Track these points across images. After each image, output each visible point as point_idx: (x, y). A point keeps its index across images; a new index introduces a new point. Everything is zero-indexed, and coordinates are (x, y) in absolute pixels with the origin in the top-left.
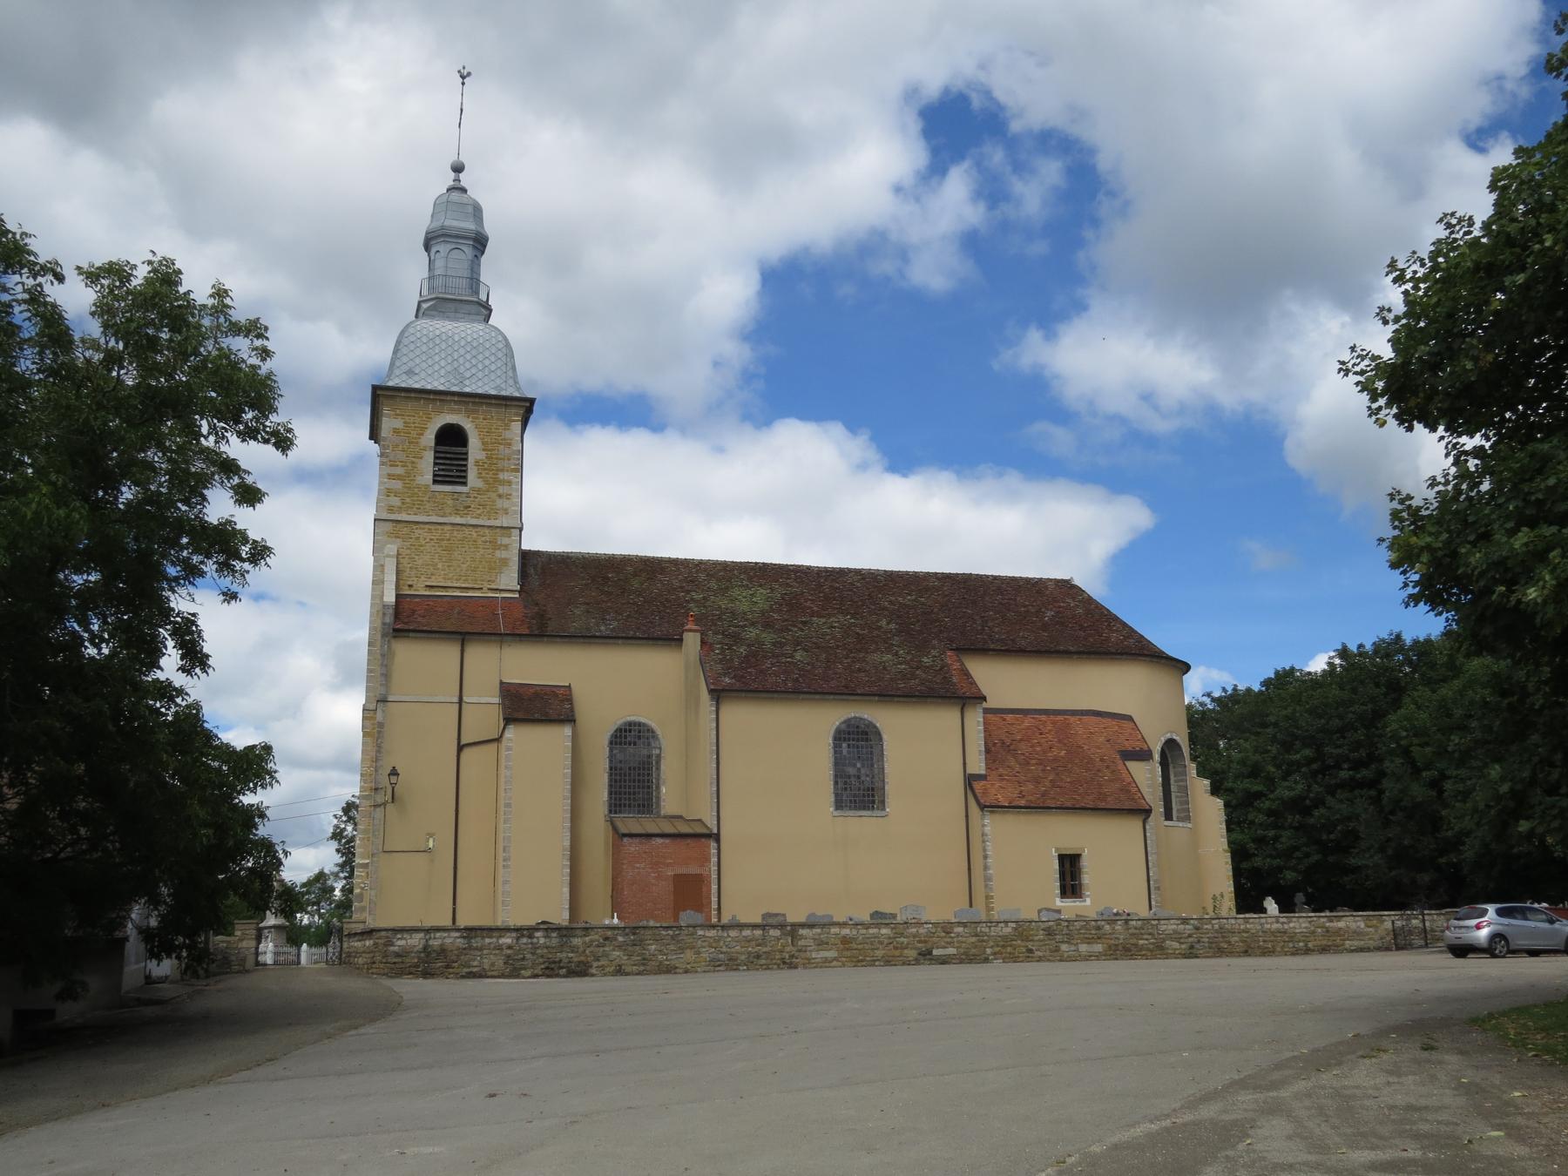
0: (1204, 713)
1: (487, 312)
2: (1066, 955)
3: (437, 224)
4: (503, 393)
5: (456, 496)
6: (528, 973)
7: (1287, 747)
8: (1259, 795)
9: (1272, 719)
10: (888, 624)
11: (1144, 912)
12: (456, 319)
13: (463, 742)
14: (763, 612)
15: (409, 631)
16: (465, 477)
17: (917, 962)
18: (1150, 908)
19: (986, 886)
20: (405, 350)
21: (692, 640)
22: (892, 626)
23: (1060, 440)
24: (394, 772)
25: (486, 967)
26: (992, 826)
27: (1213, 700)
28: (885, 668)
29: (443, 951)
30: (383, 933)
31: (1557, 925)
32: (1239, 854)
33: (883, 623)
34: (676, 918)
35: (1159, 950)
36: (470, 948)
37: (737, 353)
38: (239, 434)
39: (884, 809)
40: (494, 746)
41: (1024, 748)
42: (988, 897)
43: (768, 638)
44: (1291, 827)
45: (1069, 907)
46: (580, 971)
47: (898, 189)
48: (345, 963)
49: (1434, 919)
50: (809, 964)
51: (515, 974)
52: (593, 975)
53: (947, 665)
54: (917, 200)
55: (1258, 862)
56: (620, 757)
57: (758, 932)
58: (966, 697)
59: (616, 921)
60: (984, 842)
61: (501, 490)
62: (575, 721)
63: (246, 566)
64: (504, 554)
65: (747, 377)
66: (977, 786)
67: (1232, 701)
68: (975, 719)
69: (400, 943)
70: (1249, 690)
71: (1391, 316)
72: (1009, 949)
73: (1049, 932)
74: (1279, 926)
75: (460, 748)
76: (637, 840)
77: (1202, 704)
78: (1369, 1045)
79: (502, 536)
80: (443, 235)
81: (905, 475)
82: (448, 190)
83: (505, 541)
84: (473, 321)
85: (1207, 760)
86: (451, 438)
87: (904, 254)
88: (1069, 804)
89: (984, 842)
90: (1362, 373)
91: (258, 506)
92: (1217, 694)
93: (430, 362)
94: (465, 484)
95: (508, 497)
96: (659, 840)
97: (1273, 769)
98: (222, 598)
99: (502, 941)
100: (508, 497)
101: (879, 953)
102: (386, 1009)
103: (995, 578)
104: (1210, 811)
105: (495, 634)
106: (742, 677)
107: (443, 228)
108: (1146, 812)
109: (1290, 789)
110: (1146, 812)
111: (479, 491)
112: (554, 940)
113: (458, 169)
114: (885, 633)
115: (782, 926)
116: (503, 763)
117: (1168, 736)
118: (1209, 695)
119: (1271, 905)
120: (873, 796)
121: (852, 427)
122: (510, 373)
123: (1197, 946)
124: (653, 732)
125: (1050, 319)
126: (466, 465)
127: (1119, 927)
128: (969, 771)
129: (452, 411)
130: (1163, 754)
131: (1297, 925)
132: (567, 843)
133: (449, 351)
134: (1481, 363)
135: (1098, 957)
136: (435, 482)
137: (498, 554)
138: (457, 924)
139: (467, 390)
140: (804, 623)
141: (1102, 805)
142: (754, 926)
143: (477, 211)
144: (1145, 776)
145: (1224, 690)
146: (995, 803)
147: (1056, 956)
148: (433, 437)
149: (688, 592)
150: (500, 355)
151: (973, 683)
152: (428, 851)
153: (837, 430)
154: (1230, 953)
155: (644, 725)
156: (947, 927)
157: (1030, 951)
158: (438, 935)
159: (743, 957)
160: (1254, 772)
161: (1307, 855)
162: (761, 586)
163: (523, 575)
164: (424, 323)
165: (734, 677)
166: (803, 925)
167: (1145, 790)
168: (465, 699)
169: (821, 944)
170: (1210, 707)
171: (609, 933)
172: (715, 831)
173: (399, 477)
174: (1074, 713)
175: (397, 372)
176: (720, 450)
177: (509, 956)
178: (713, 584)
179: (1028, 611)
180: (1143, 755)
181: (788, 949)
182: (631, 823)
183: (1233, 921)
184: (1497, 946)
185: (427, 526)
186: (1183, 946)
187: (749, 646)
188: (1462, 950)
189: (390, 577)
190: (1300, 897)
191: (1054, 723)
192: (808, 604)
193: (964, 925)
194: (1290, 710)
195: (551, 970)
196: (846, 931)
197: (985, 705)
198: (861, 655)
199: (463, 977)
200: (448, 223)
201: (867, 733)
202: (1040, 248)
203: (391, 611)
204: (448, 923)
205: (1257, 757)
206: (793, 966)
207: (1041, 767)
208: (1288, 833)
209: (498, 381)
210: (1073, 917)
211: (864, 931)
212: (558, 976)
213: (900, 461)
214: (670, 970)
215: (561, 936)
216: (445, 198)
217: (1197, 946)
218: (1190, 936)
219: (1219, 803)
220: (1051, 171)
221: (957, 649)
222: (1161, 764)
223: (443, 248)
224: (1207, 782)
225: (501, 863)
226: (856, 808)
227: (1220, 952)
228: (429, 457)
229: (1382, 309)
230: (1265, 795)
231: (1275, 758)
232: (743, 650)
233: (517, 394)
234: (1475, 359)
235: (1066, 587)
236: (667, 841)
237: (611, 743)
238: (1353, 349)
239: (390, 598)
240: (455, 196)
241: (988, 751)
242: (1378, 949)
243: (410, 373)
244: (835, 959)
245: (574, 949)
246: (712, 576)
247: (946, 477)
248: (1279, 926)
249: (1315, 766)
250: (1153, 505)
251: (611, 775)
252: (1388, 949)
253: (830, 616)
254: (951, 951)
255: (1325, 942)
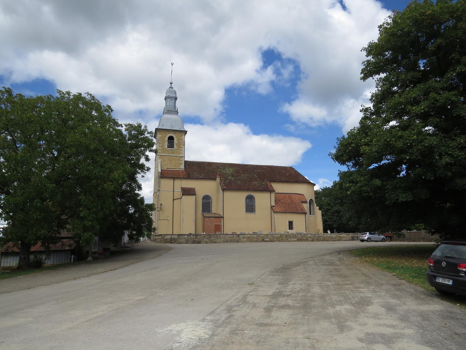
0: (319, 192)
1: (177, 113)
2: (289, 241)
3: (167, 95)
4: (181, 130)
5: (172, 150)
6: (190, 243)
7: (335, 200)
8: (330, 209)
9: (333, 194)
10: (256, 176)
11: (305, 233)
12: (171, 114)
13: (174, 199)
14: (232, 173)
15: (164, 177)
16: (174, 146)
17: (261, 241)
18: (306, 232)
19: (275, 227)
20: (162, 121)
21: (218, 179)
22: (257, 176)
23: (292, 128)
24: (161, 205)
25: (182, 242)
26: (276, 215)
27: (322, 189)
28: (256, 185)
29: (174, 239)
30: (163, 235)
31: (380, 236)
32: (324, 222)
33: (255, 176)
34: (215, 233)
35: (307, 240)
36: (179, 238)
37: (220, 108)
38: (149, 151)
39: (255, 212)
40: (180, 199)
41: (282, 201)
42: (275, 229)
43: (233, 179)
44: (336, 216)
45: (290, 231)
46: (199, 242)
47: (257, 71)
48: (154, 241)
49: (359, 235)
50: (241, 242)
51: (187, 243)
52: (202, 243)
53: (268, 184)
54: (261, 73)
55: (329, 223)
56: (204, 202)
57: (232, 236)
58: (271, 191)
59: (205, 233)
60: (274, 219)
61: (181, 149)
62: (196, 195)
63: (146, 171)
64: (181, 162)
65: (222, 113)
66: (273, 208)
67: (325, 190)
68: (273, 195)
69: (166, 237)
70: (329, 188)
71: (336, 147)
72: (279, 239)
73: (286, 236)
74: (330, 236)
75: (174, 200)
76: (208, 218)
77: (319, 190)
78: (331, 254)
79: (181, 158)
80: (169, 97)
81: (258, 136)
82: (169, 88)
83: (182, 159)
84: (175, 115)
85: (319, 202)
86: (171, 138)
87: (257, 85)
88: (291, 212)
89: (274, 219)
90: (332, 156)
91: (149, 161)
92: (322, 188)
93: (167, 123)
94: (174, 148)
95: (182, 150)
96: (212, 218)
97: (332, 204)
98: (141, 177)
99: (185, 237)
100: (182, 150)
101: (254, 240)
102: (170, 249)
103: (277, 166)
104: (318, 213)
105: (180, 178)
106: (228, 186)
107: (169, 96)
108: (306, 213)
109: (336, 208)
110: (306, 213)
111: (176, 149)
112: (194, 237)
113: (171, 83)
114: (256, 178)
115: (236, 235)
116: (182, 203)
117: (311, 198)
118: (321, 188)
119: (329, 232)
120: (253, 210)
121: (245, 125)
122: (182, 126)
123: (314, 239)
124: (211, 197)
125: (290, 100)
126: (174, 144)
127: (299, 235)
128: (271, 205)
129: (171, 133)
130: (310, 202)
131: (333, 236)
132: (194, 218)
133: (170, 121)
134: (346, 158)
135: (295, 241)
136: (168, 147)
137: (180, 162)
138: (173, 234)
139: (174, 129)
140: (240, 176)
141: (297, 212)
142: (231, 235)
143: (175, 93)
144: (306, 206)
145: (324, 187)
146: (276, 211)
147: (287, 241)
148: (167, 138)
149: (217, 169)
150: (180, 122)
151: (273, 188)
152: (167, 220)
153: (242, 125)
154: (321, 241)
155: (209, 196)
156: (267, 235)
157: (283, 240)
158: (173, 236)
159: (229, 240)
160: (329, 205)
161: (339, 222)
162: (231, 168)
163: (185, 166)
164: (165, 115)
165: (226, 187)
166: (240, 235)
167: (306, 209)
168: (174, 190)
169: (244, 238)
170: (321, 191)
171: (204, 236)
172: (223, 216)
173: (161, 146)
174: (292, 194)
175: (160, 125)
176: (216, 129)
177: (186, 240)
178: (222, 168)
179: (284, 173)
180: (306, 202)
181: (237, 239)
182: (206, 215)
183: (321, 235)
184: (369, 240)
185: (167, 156)
186: (312, 239)
187: (229, 180)
188: (362, 241)
189: (160, 166)
190: (335, 230)
191: (288, 196)
192: (241, 172)
193: (270, 235)
194: (336, 192)
195: (194, 242)
196: (248, 236)
197: (275, 192)
198: (251, 182)
199: (178, 243)
200: (170, 95)
201: (252, 198)
202: (288, 85)
203: (160, 173)
204: (172, 233)
205: (330, 202)
206: (238, 242)
207: (285, 204)
208: (335, 217)
209: (180, 127)
210: (291, 233)
211: (252, 236)
212: (195, 243)
213: (256, 132)
214: (216, 242)
215: (195, 236)
216: (169, 90)
217: (314, 239)
218: (313, 237)
219: (320, 211)
220: (291, 68)
221: (270, 181)
222: (309, 204)
223: (169, 100)
224: (318, 207)
225: (182, 222)
226: (250, 212)
227: (318, 240)
228: (167, 142)
229: (335, 146)
230: (331, 209)
231: (333, 202)
232: (228, 181)
233: (184, 130)
234: (345, 158)
235: (291, 168)
236: (214, 218)
237: (202, 199)
238: (330, 153)
239: (160, 171)
240: (171, 89)
241: (275, 201)
242: (349, 240)
243: (163, 126)
244: (246, 241)
245: (198, 239)
246: (222, 166)
247: (266, 136)
248: (330, 236)
249: (341, 204)
250: (311, 143)
251: (202, 205)
252: (351, 240)
253: (245, 174)
254: (268, 239)
255: (338, 239)
